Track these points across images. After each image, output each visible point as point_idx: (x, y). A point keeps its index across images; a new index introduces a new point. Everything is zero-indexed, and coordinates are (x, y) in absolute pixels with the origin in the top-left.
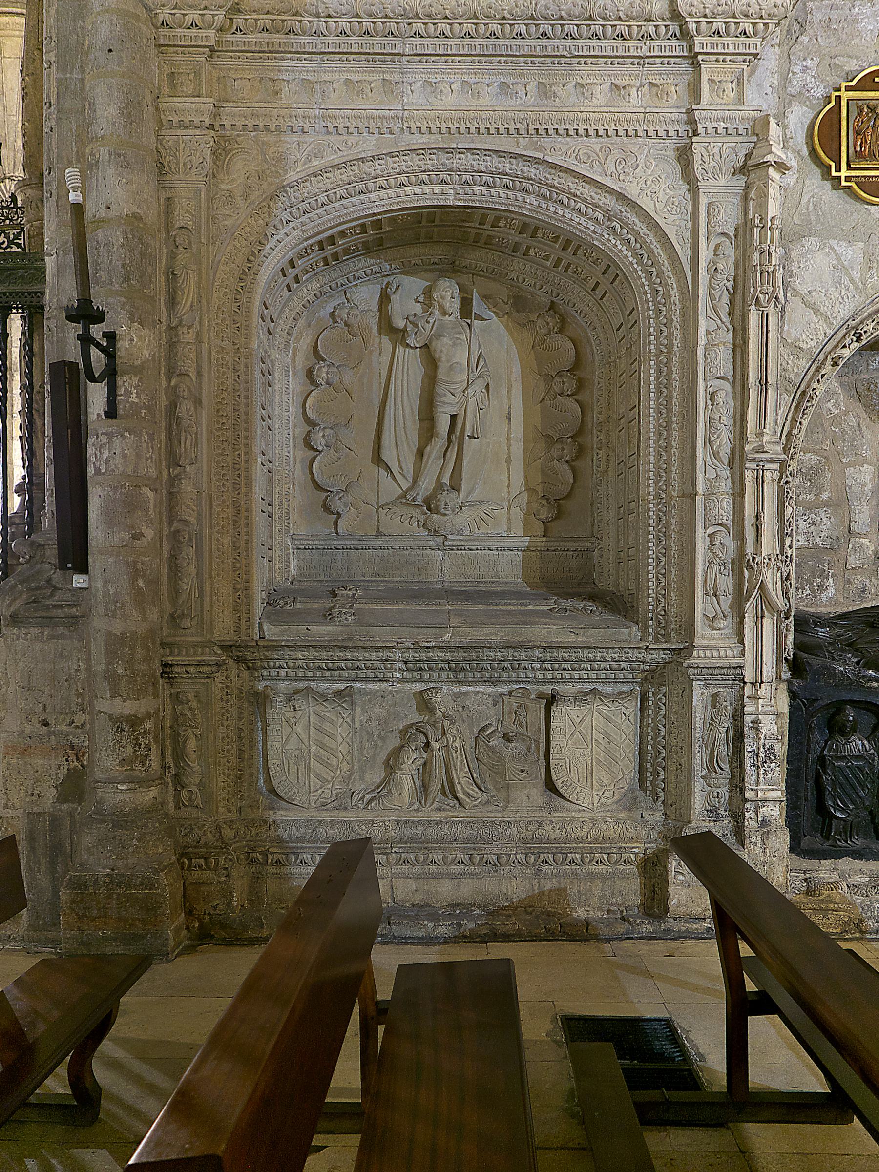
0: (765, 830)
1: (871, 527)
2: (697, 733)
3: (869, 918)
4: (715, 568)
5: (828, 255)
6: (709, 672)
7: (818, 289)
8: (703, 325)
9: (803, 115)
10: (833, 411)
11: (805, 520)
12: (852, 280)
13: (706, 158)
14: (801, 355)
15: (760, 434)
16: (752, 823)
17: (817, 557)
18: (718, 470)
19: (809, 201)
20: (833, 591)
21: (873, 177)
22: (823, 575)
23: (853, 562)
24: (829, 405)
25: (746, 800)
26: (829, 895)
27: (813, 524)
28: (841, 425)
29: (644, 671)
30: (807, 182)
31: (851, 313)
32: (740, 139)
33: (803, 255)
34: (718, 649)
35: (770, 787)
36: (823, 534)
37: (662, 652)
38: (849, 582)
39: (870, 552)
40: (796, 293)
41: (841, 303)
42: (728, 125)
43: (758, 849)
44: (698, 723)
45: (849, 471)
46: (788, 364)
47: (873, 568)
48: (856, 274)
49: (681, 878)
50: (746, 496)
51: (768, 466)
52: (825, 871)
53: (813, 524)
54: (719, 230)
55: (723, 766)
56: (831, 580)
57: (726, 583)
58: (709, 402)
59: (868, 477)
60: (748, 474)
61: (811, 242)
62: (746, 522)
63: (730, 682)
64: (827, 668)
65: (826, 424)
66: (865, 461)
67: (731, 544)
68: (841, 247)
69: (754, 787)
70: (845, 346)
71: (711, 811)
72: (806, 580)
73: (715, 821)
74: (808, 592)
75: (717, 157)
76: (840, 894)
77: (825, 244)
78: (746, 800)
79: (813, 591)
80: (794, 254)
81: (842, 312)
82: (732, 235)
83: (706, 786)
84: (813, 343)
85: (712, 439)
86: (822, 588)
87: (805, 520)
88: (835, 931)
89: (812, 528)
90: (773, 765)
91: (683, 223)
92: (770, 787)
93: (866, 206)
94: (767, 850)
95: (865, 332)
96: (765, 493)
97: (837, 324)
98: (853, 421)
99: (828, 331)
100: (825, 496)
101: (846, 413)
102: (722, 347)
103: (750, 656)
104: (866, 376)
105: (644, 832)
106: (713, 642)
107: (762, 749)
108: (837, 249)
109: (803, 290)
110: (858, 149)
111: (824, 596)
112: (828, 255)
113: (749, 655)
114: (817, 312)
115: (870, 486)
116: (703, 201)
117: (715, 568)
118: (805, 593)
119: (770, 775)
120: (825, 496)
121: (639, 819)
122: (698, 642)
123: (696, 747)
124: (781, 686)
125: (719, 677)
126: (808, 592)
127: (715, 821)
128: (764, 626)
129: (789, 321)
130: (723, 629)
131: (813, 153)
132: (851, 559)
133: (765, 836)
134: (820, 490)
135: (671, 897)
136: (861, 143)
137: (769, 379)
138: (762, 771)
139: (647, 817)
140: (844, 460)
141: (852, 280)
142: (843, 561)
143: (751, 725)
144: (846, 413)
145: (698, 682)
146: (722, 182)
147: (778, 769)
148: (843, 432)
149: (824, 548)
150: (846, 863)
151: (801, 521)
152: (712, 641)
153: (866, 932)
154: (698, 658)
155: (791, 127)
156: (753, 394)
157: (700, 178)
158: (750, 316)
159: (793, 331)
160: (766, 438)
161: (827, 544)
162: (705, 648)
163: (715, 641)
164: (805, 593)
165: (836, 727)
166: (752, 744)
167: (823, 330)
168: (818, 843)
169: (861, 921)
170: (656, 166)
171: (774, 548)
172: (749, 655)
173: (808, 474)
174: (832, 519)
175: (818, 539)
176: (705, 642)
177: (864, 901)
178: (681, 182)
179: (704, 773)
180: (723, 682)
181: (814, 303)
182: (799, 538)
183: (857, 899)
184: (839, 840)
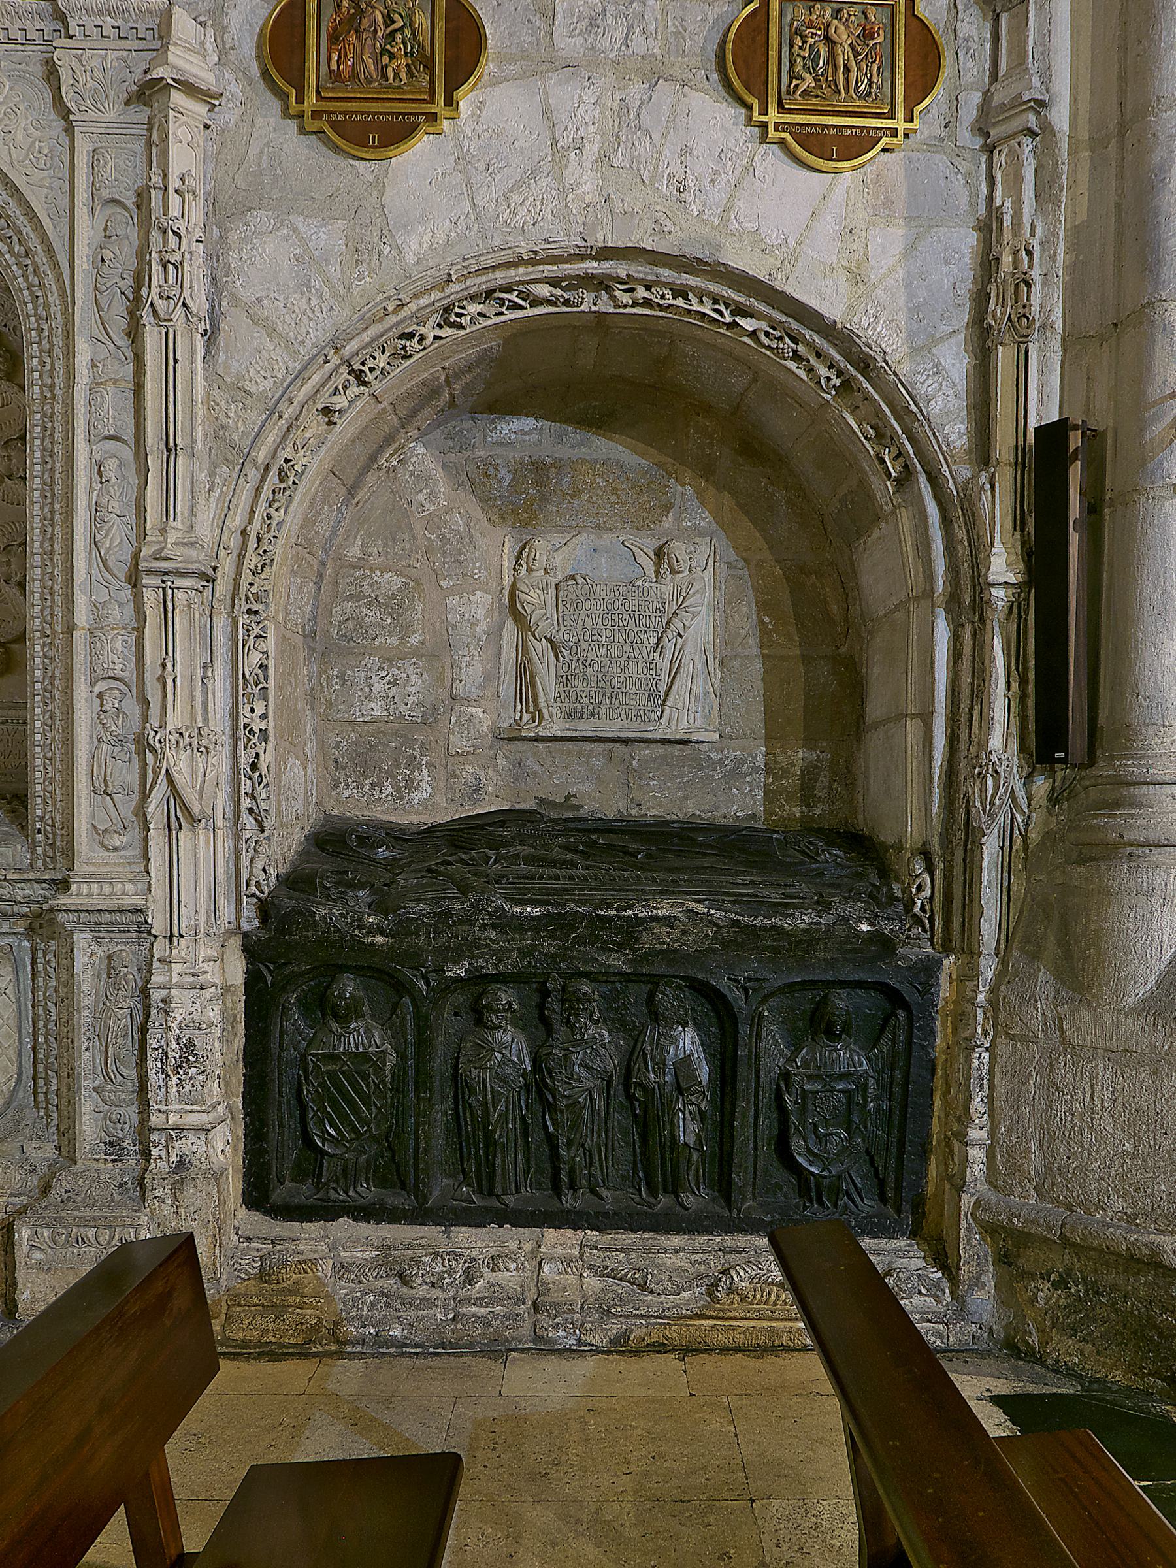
0: (177, 1177)
1: (484, 688)
2: (84, 1017)
3: (350, 1320)
4: (105, 748)
5: (285, 239)
6: (98, 920)
7: (272, 295)
8: (83, 352)
9: (253, 11)
10: (427, 506)
11: (383, 678)
12: (327, 281)
13: (79, 75)
14: (249, 403)
15: (163, 531)
16: (162, 1165)
17: (402, 735)
18: (112, 588)
19: (261, 152)
20: (429, 790)
21: (356, 113)
22: (413, 764)
23: (458, 742)
24: (420, 497)
25: (151, 1130)
26: (297, 1282)
27: (394, 683)
28: (439, 528)
29: (25, 916)
30: (258, 120)
31: (329, 336)
32: (141, 45)
33: (246, 240)
34: (110, 881)
35: (188, 1107)
36: (410, 700)
37: (36, 886)
38: (453, 775)
39: (485, 728)
40: (236, 302)
41: (311, 319)
42: (119, 23)
43: (167, 1209)
44: (85, 1001)
45: (454, 601)
46: (228, 417)
47: (491, 753)
48: (334, 272)
49: (37, 1255)
50: (147, 630)
51: (179, 582)
52: (307, 1238)
53: (394, 683)
54: (106, 194)
55: (124, 1071)
56: (425, 773)
57: (126, 773)
58: (96, 477)
59: (481, 612)
60: (148, 594)
61: (261, 218)
62: (147, 675)
63: (135, 935)
64: (300, 913)
65: (417, 527)
66: (478, 585)
67: (132, 707)
68: (308, 227)
69: (162, 1107)
70: (336, 392)
71: (111, 1144)
72: (387, 772)
73: (114, 1161)
74: (390, 790)
75: (99, 74)
76: (318, 1278)
77: (282, 221)
78: (151, 1130)
79: (397, 789)
80: (233, 237)
81: (316, 333)
82: (129, 203)
83: (102, 1104)
84: (268, 384)
85: (98, 537)
86: (411, 785)
87: (383, 678)
88: (292, 1341)
89: (394, 690)
90: (192, 1071)
91: (57, 184)
92: (188, 1107)
93: (352, 162)
94: (182, 1210)
95: (372, 370)
96: (177, 627)
97: (305, 352)
98: (459, 523)
99: (290, 364)
100: (414, 640)
101: (449, 510)
102: (110, 388)
103: (160, 893)
104: (482, 453)
105: (18, 1177)
106: (104, 870)
107: (174, 1045)
108: (303, 230)
109: (248, 295)
110: (334, 67)
111: (415, 798)
112: (285, 239)
113: (159, 891)
114: (272, 332)
115: (484, 626)
116: (83, 147)
117: (105, 748)
118: (385, 792)
119: (187, 1088)
120: (414, 640)
121: (18, 1154)
122: (80, 868)
123: (82, 1041)
124: (232, 941)
125: (111, 927)
126: (390, 790)
127: (114, 1161)
128: (181, 843)
129: (227, 345)
130: (123, 848)
131: (265, 74)
132: (455, 739)
133: (178, 1187)
134: (406, 630)
135: (20, 1286)
136: (340, 58)
137: (179, 441)
138: (174, 1080)
139: (31, 1151)
140: (444, 584)
141: (327, 281)
142: (443, 743)
143: (161, 1005)
144: (449, 510)
145: (83, 936)
146: (111, 115)
147: (201, 1077)
148: (445, 541)
149: (413, 722)
150: (343, 1227)
151: (376, 679)
152: (101, 868)
153: (346, 1343)
154: (79, 895)
155: (234, 30)
156: (154, 463)
157: (73, 108)
158: (147, 335)
159: (234, 365)
160: (172, 537)
161: (418, 715)
162: (88, 879)
163: (108, 869)
164: (385, 792)
165: (324, 1008)
166: (158, 1036)
167: (283, 363)
168: (304, 1193)
169: (337, 1324)
170: (11, 89)
171: (193, 717)
172: (159, 891)
173: (387, 605)
174: (425, 676)
175: (402, 708)
176: (91, 869)
177: (352, 1291)
178: (53, 116)
179: (97, 1083)
180: (123, 935)
181: (267, 318)
182: (373, 705)
183: (343, 1288)
184: (335, 1190)
